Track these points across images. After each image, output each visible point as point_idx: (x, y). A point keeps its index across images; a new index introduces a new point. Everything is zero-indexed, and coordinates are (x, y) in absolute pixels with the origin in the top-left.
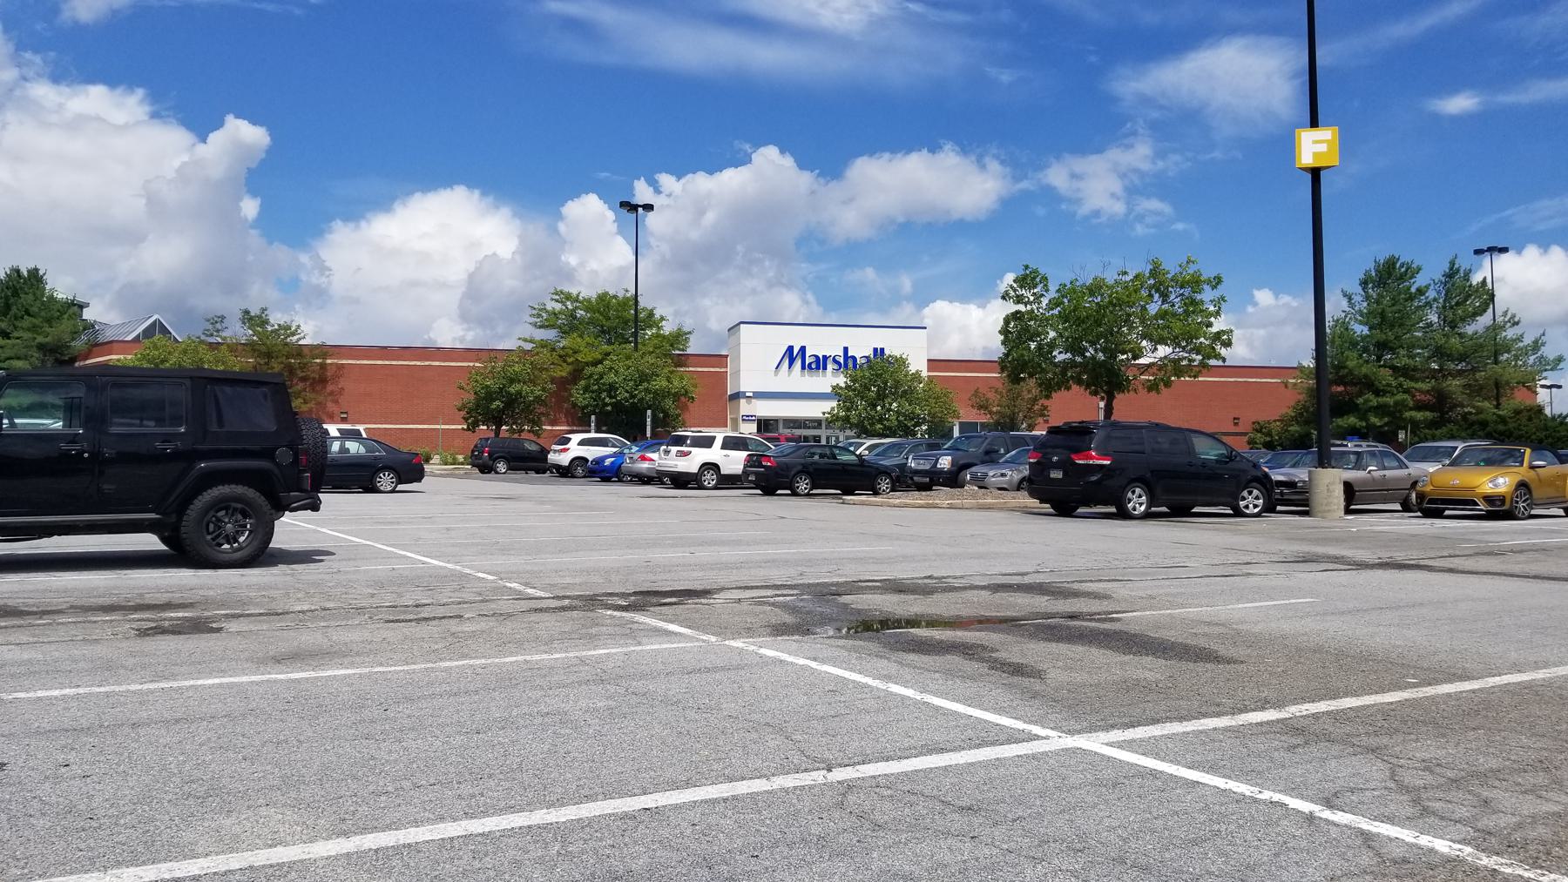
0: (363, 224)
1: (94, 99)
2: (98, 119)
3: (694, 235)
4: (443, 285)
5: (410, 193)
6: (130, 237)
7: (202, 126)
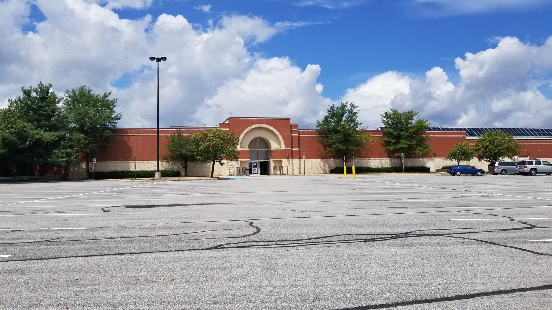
0: (357, 88)
1: (275, 62)
3: (481, 74)
5: (372, 76)
6: (285, 103)
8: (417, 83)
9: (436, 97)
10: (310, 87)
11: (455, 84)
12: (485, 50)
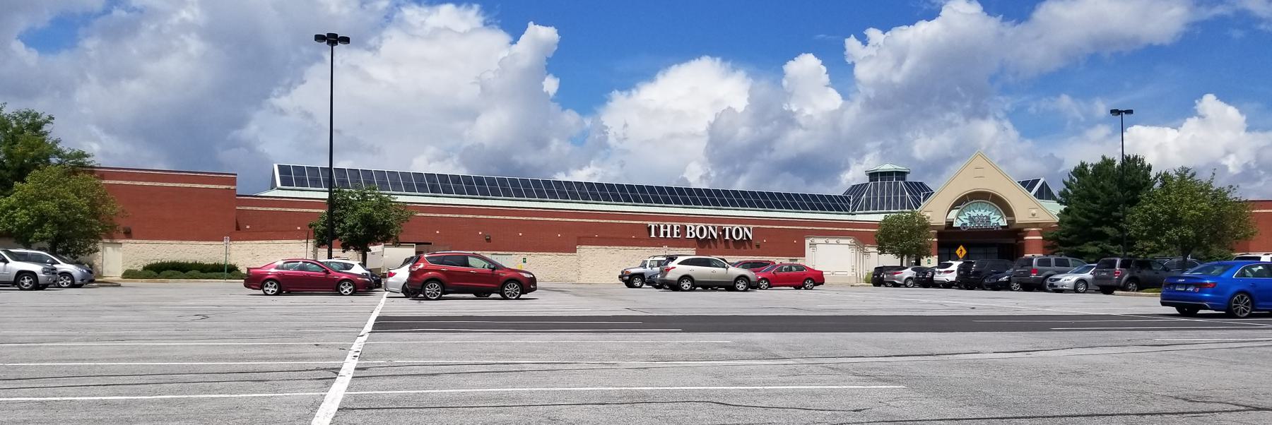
0: (634, 92)
2: (447, 29)
3: (897, 78)
4: (695, 136)
5: (668, 66)
6: (471, 114)
7: (516, 33)
8: (764, 87)
9: (802, 122)
10: (532, 77)
11: (845, 96)
12: (911, 22)
